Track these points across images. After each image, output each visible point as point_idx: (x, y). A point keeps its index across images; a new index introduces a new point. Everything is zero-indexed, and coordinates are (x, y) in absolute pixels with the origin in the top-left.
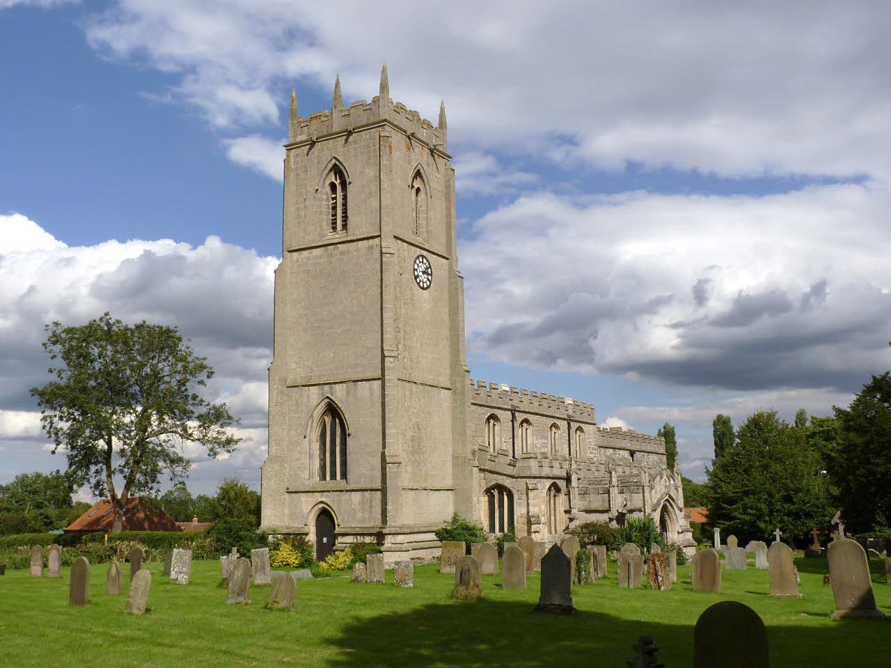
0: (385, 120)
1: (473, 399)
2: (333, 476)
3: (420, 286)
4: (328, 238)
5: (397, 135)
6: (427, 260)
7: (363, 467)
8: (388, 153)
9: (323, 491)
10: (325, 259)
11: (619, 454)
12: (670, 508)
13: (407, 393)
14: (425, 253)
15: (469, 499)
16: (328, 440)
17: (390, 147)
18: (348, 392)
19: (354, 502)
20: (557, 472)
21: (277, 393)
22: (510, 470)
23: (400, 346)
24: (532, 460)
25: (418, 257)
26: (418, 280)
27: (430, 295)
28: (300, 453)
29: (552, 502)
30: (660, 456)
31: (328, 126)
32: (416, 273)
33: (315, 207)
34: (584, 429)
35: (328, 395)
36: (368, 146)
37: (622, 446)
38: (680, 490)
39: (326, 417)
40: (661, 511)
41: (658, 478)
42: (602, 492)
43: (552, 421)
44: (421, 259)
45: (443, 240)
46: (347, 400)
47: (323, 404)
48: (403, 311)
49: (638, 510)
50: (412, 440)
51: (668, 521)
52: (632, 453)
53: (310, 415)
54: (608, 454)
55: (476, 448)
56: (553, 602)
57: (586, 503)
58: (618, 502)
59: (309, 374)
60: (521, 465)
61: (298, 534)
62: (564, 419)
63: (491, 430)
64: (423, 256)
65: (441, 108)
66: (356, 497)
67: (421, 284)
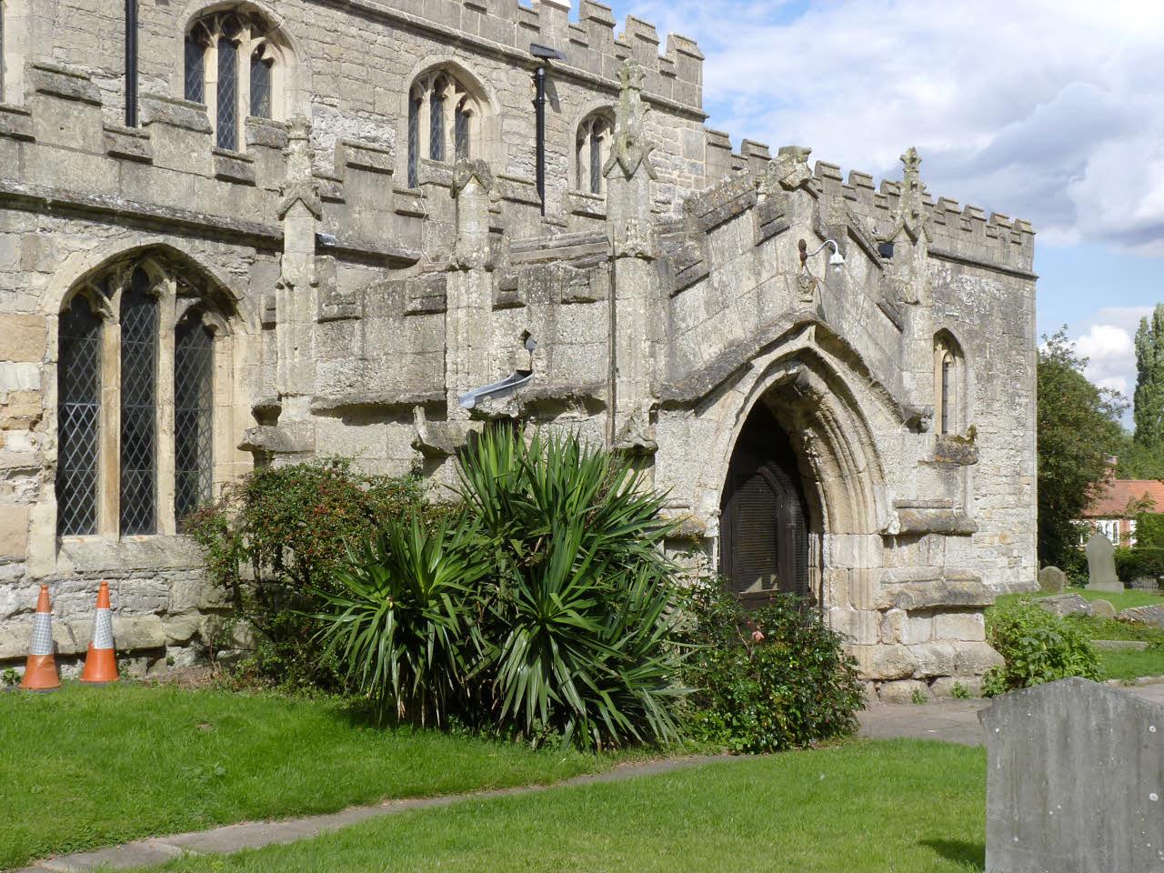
2: (137, 515)
12: (831, 401)
30: (1012, 279)
40: (113, 261)
42: (416, 304)
43: (436, 54)
49: (578, 401)
51: (830, 477)
57: (347, 368)
58: (480, 353)
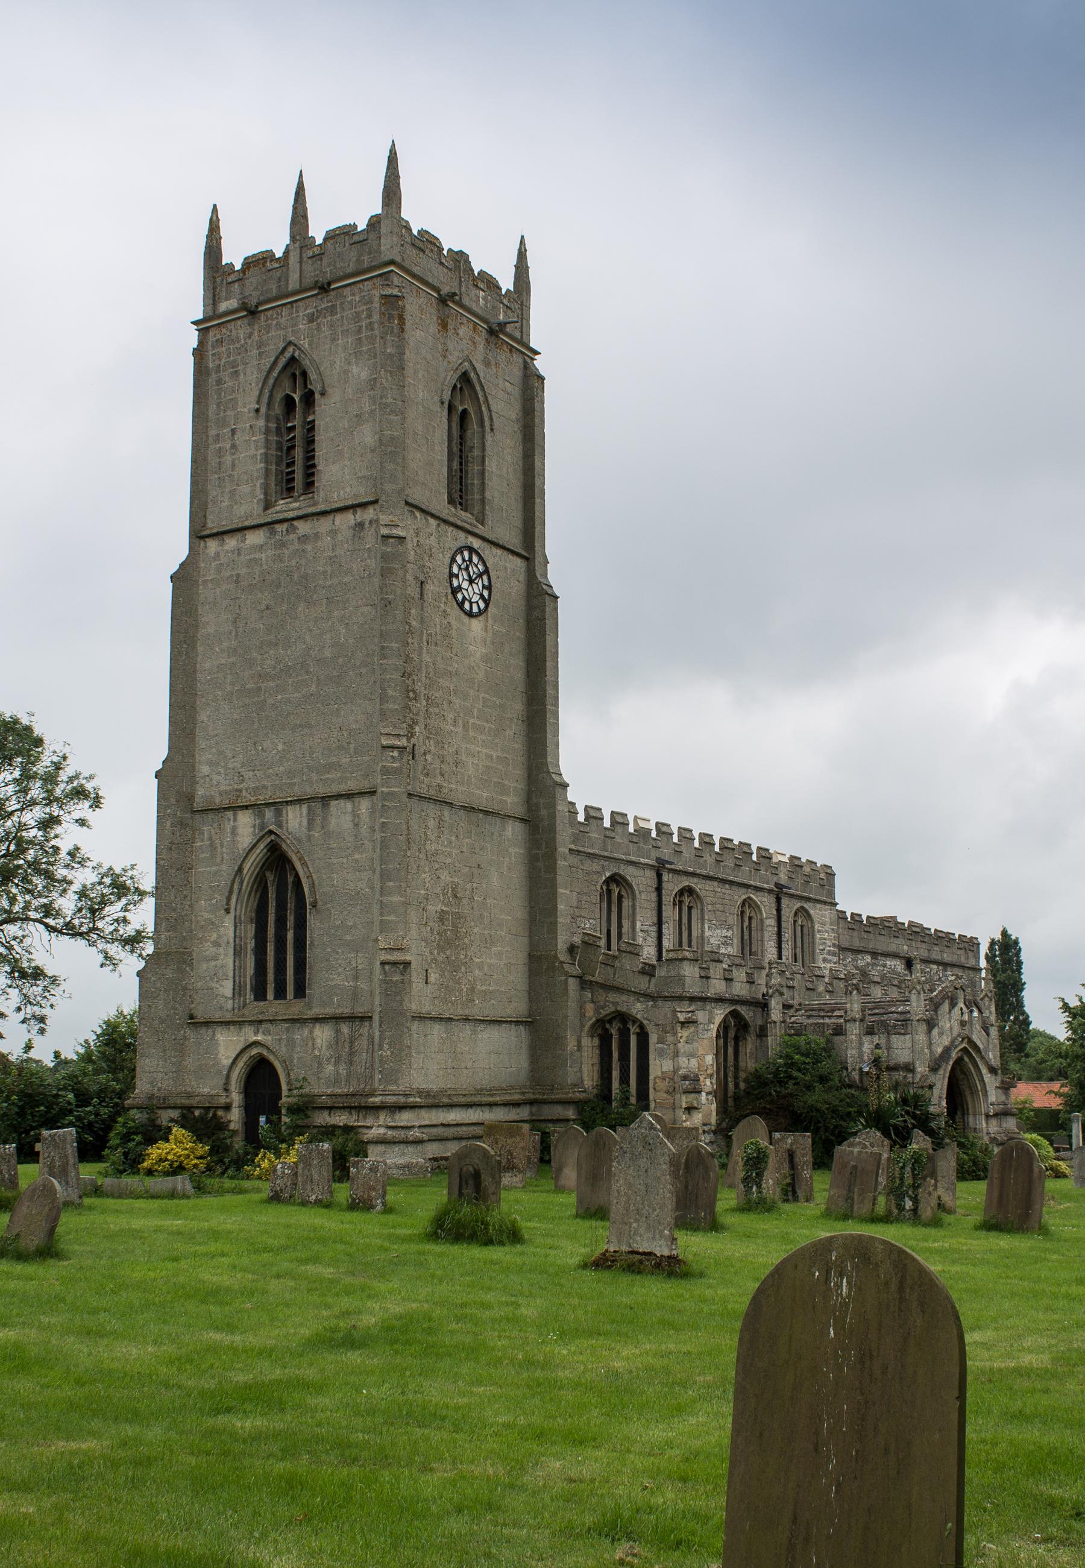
0: (392, 262)
1: (573, 842)
2: (280, 993)
4: (278, 508)
5: (418, 296)
6: (481, 558)
7: (338, 968)
8: (396, 331)
9: (261, 1022)
10: (270, 553)
11: (885, 966)
13: (432, 824)
14: (476, 543)
15: (559, 1041)
17: (401, 318)
18: (311, 822)
19: (319, 1041)
20: (740, 989)
21: (173, 825)
22: (642, 984)
23: (417, 729)
24: (685, 963)
25: (460, 551)
26: (460, 596)
27: (486, 630)
29: (730, 1050)
31: (279, 279)
32: (455, 583)
33: (253, 446)
34: (812, 912)
35: (272, 827)
36: (357, 317)
37: (892, 948)
38: (994, 1032)
39: (268, 874)
41: (946, 1006)
45: (516, 518)
46: (309, 837)
47: (262, 846)
48: (426, 658)
50: (441, 920)
52: (909, 964)
53: (236, 868)
54: (861, 963)
55: (577, 940)
56: (635, 1247)
59: (236, 787)
60: (663, 974)
61: (208, 1109)
62: (770, 891)
63: (614, 908)
64: (471, 550)
65: (520, 250)
66: (323, 1035)
67: (467, 606)
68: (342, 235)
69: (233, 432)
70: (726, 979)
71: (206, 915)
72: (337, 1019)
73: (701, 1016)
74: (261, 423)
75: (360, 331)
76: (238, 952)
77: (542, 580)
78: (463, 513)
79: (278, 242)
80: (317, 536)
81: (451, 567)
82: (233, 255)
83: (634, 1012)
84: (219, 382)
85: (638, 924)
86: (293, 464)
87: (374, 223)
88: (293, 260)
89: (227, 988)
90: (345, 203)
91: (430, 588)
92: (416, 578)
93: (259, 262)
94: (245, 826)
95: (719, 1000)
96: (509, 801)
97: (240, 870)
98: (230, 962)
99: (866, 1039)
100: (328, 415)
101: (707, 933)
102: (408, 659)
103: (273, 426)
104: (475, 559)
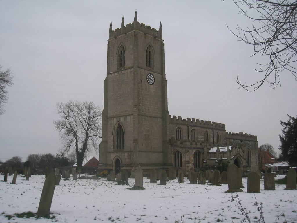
2: (120, 148)
3: (150, 84)
6: (153, 75)
7: (128, 144)
13: (144, 120)
14: (152, 73)
16: (119, 136)
26: (149, 82)
28: (111, 140)
32: (148, 80)
37: (238, 138)
44: (150, 75)
52: (242, 141)
64: (151, 74)
65: (160, 24)
66: (126, 154)
67: (150, 83)
68: (129, 25)
69: (113, 57)
70: (196, 145)
71: (110, 135)
72: (128, 152)
73: (190, 151)
74: (117, 56)
75: (131, 40)
76: (114, 141)
77: (164, 78)
78: (150, 68)
79: (120, 27)
80: (125, 73)
81: (147, 77)
82: (114, 29)
83: (179, 150)
84: (111, 49)
85: (184, 135)
86: (122, 64)
87: (133, 23)
88: (122, 30)
89: (112, 147)
90: (129, 20)
91: (143, 81)
92: (140, 80)
93: (117, 30)
94: (115, 120)
95: (194, 148)
96: (159, 115)
97: (114, 128)
98: (113, 142)
99: (220, 154)
100: (127, 54)
101: (198, 137)
102: (139, 93)
103: (119, 56)
104: (151, 75)
